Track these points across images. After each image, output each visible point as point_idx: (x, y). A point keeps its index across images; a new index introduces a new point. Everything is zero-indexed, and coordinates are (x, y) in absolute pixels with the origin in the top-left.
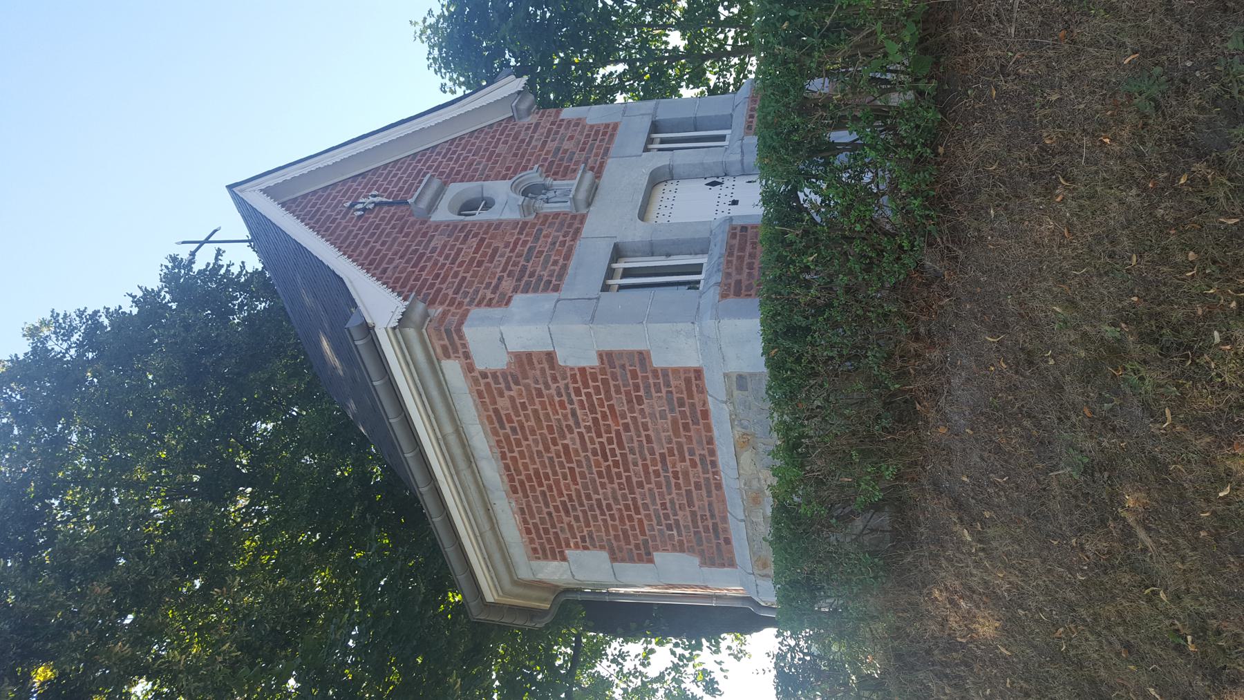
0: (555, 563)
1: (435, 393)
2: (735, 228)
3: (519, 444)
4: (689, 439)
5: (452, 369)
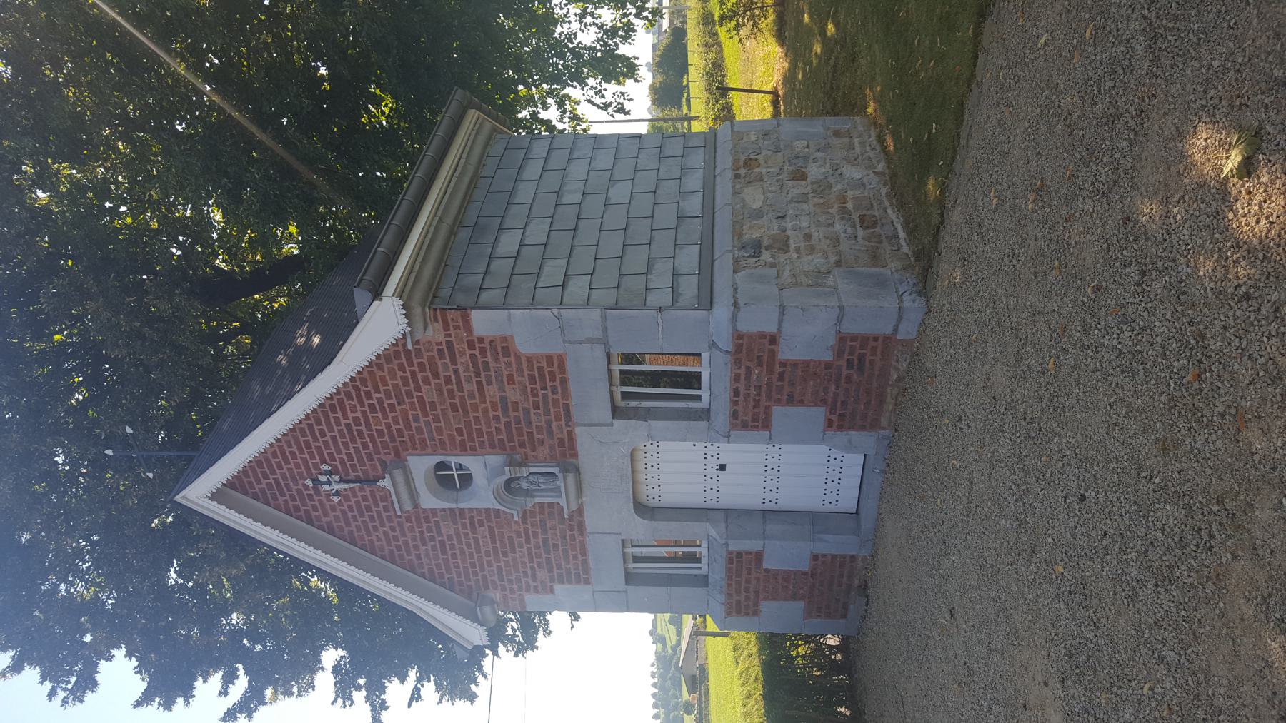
2: (731, 553)
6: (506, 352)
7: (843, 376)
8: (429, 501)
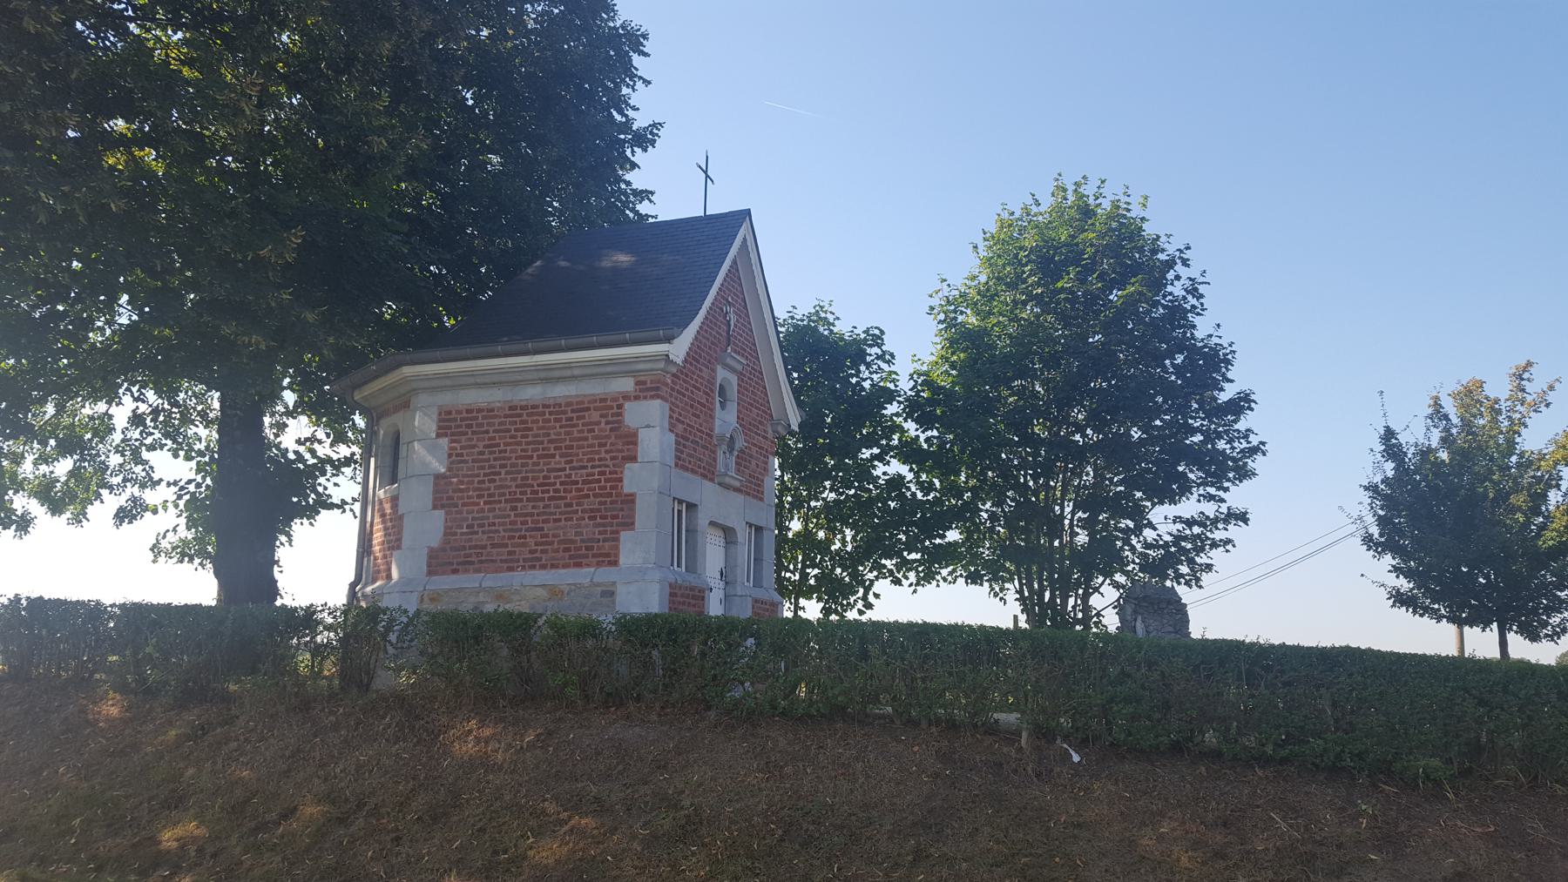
0: (434, 427)
1: (609, 369)
3: (556, 420)
4: (557, 551)
5: (626, 385)
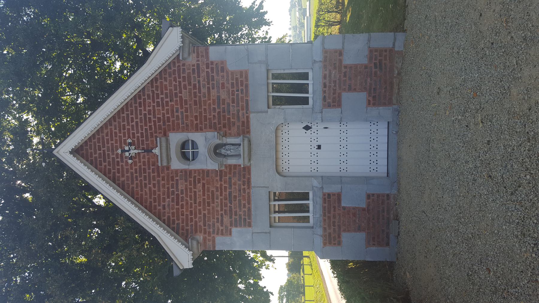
6: (223, 70)
7: (373, 73)
8: (177, 164)
